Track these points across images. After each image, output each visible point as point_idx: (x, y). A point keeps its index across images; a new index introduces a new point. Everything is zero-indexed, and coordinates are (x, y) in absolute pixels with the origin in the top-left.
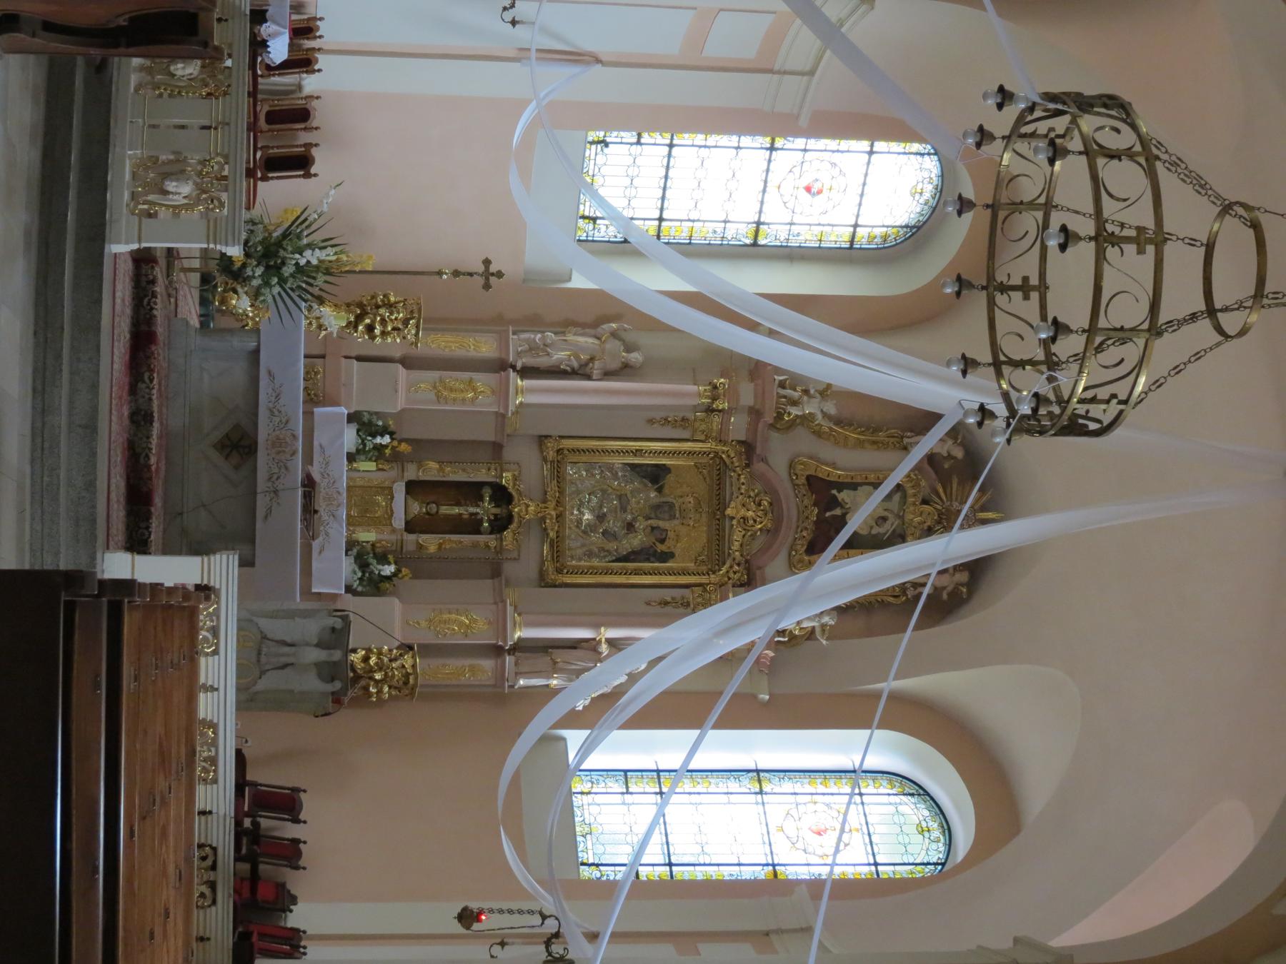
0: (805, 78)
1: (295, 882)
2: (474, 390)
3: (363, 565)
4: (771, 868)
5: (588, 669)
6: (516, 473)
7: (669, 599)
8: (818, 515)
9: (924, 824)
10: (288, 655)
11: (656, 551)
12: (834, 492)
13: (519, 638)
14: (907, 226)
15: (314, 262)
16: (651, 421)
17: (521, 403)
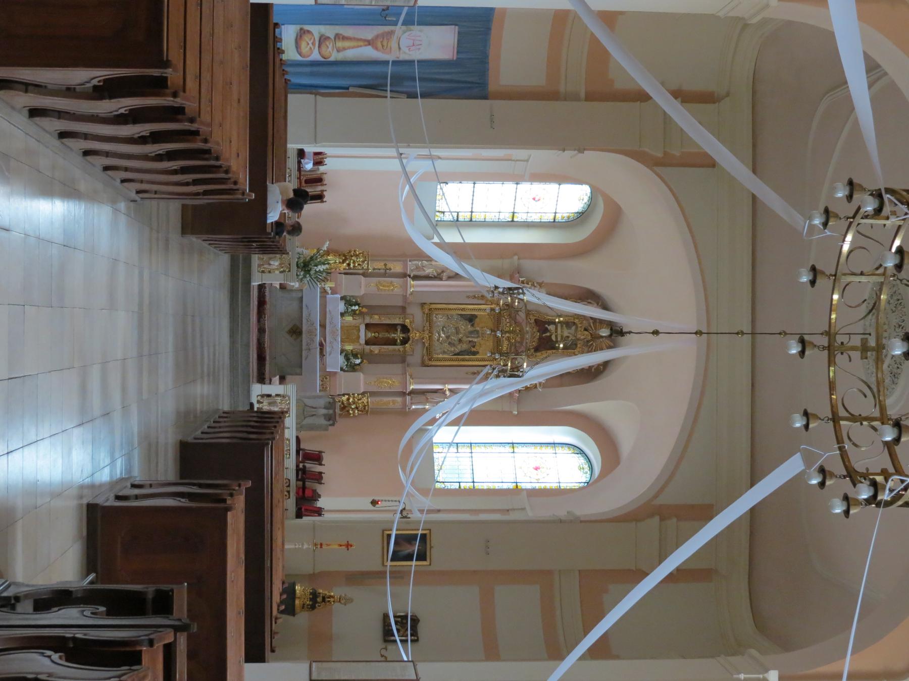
0: (525, 163)
1: (320, 489)
2: (393, 286)
3: (348, 359)
4: (515, 484)
5: (441, 401)
6: (411, 320)
7: (476, 371)
8: (539, 336)
9: (581, 466)
10: (314, 412)
11: (471, 351)
12: (547, 326)
13: (412, 389)
14: (578, 213)
15: (322, 270)
16: (468, 297)
17: (413, 291)
